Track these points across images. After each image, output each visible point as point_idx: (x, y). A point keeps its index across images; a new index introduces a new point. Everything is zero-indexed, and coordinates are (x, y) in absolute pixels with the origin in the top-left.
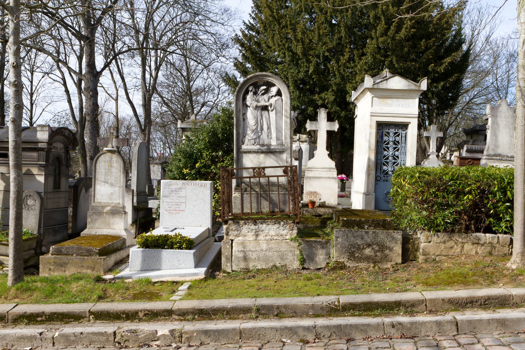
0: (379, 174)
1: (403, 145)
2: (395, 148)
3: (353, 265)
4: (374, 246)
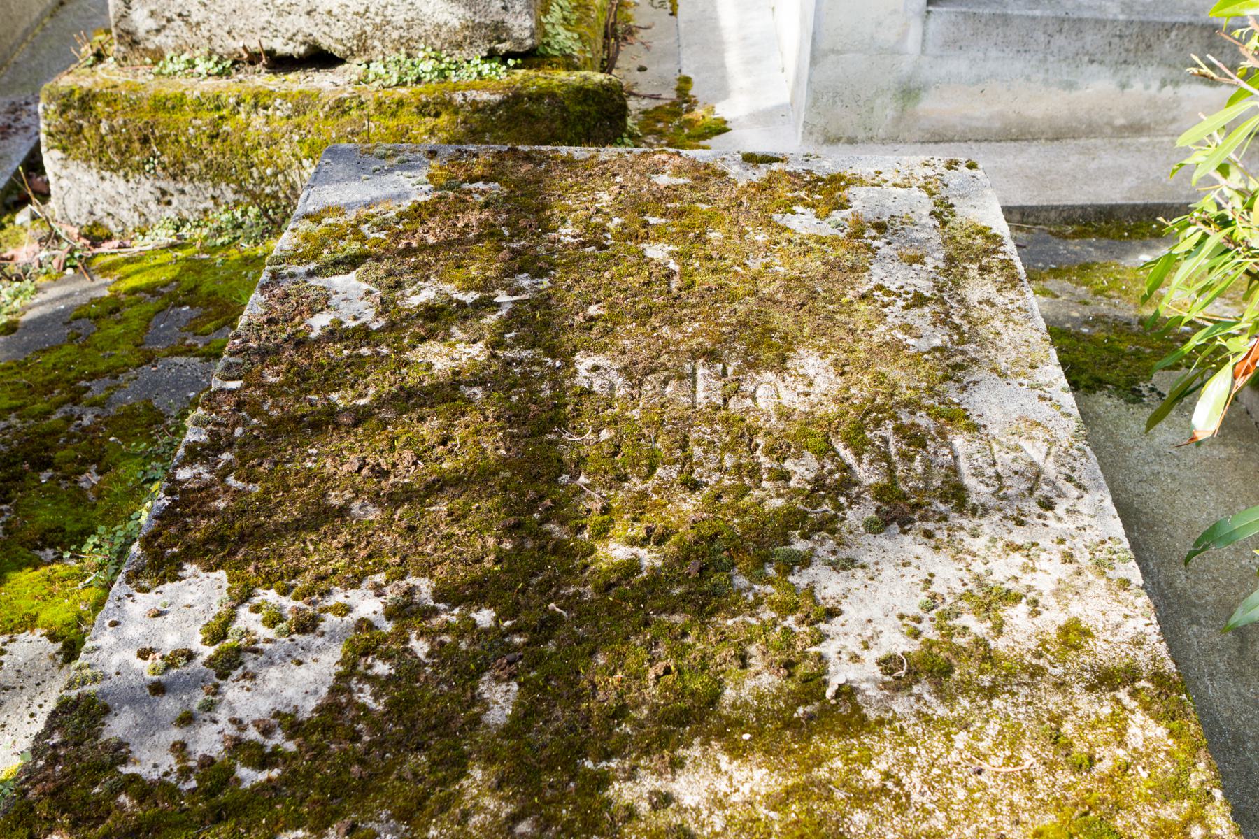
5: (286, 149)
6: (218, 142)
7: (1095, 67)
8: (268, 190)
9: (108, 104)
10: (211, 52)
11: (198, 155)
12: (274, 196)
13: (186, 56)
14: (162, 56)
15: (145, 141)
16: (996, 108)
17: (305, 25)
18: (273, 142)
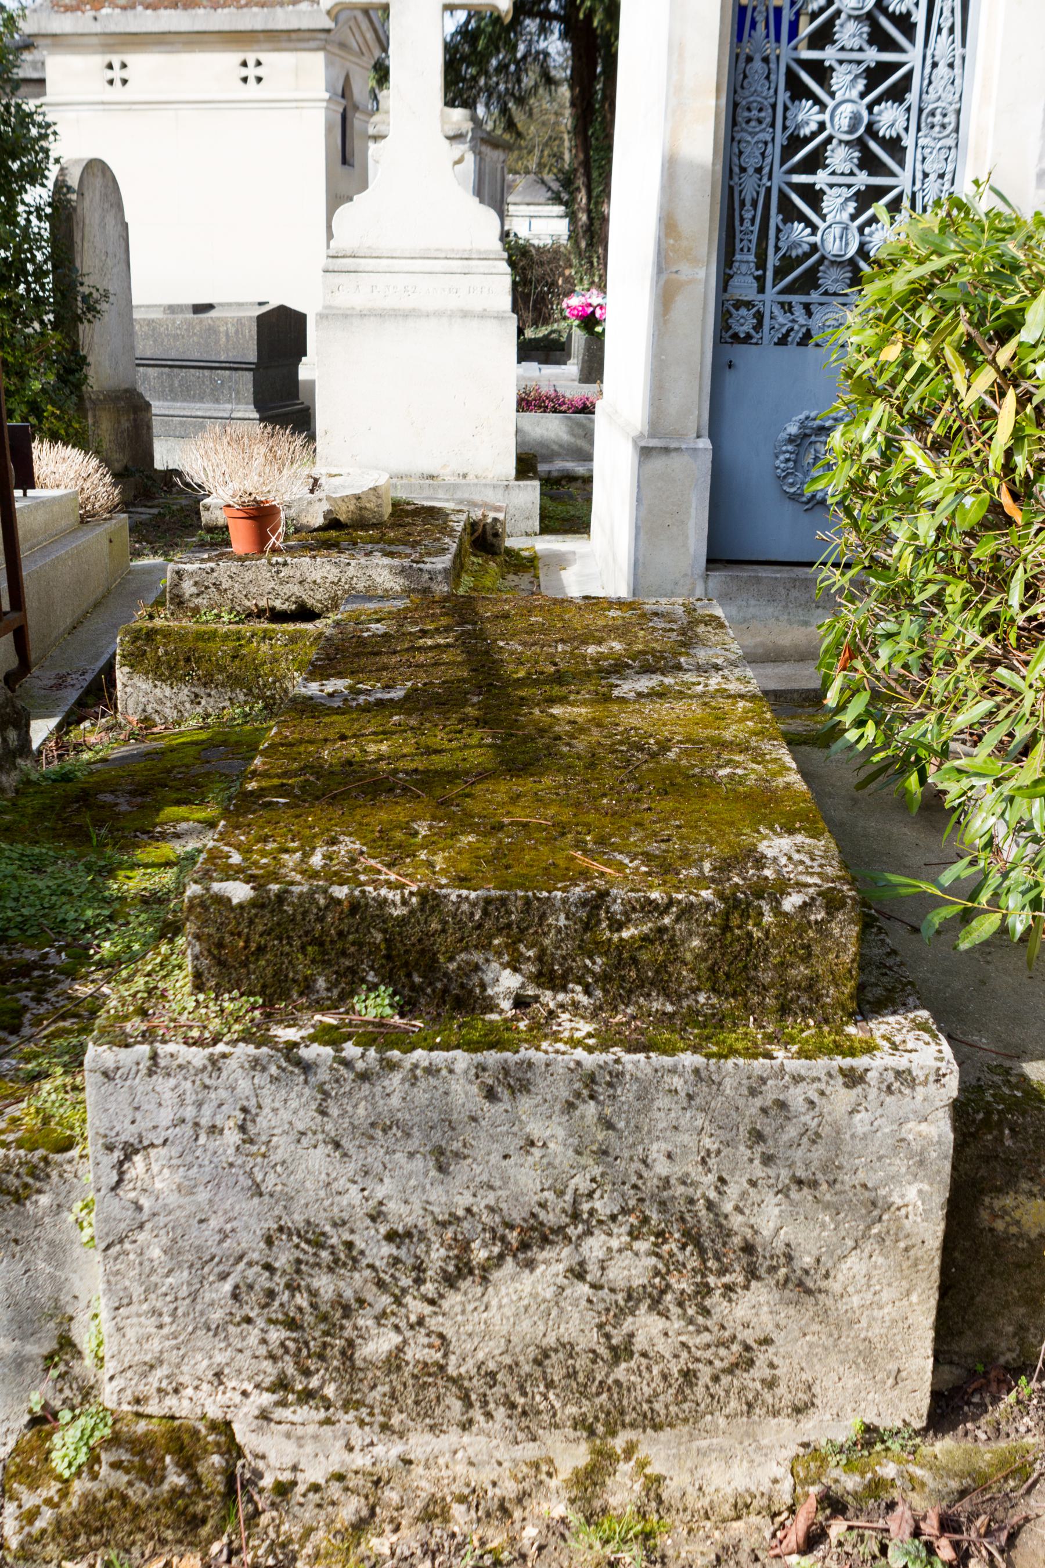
0: (744, 287)
1: (941, 45)
2: (875, 74)
3: (337, 1459)
4: (594, 1247)
5: (283, 665)
6: (237, 662)
7: (820, 611)
8: (268, 693)
9: (165, 637)
10: (232, 609)
11: (222, 669)
12: (273, 697)
13: (215, 611)
14: (199, 612)
15: (188, 660)
16: (758, 639)
17: (296, 589)
18: (275, 660)
